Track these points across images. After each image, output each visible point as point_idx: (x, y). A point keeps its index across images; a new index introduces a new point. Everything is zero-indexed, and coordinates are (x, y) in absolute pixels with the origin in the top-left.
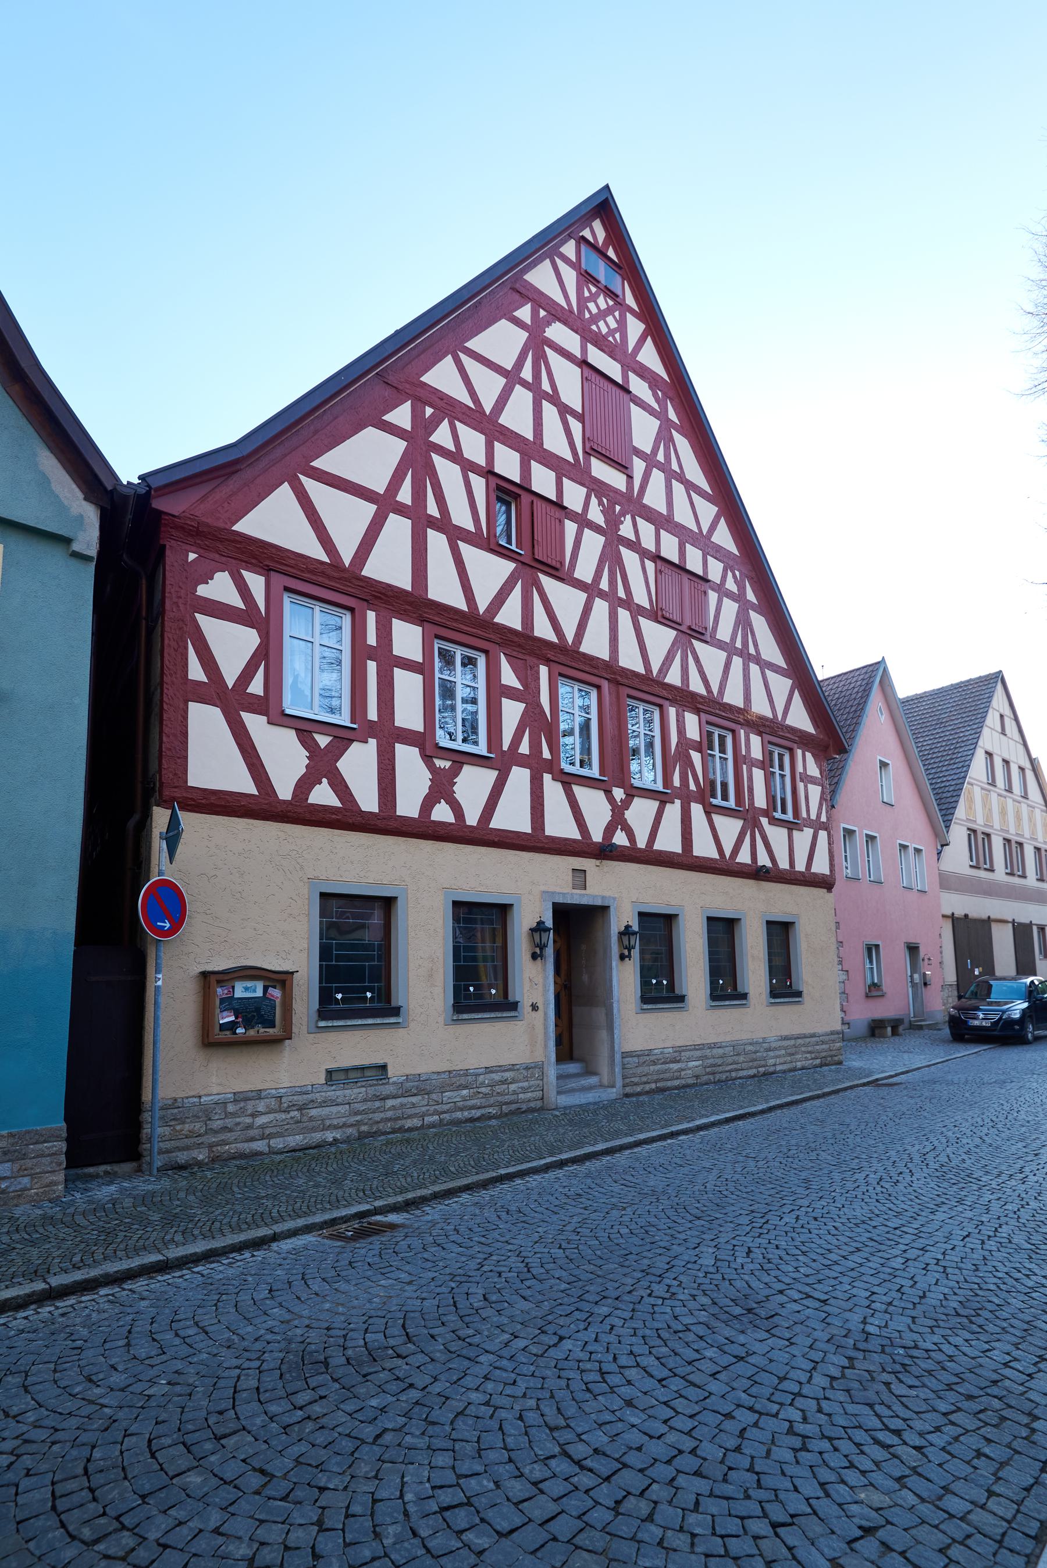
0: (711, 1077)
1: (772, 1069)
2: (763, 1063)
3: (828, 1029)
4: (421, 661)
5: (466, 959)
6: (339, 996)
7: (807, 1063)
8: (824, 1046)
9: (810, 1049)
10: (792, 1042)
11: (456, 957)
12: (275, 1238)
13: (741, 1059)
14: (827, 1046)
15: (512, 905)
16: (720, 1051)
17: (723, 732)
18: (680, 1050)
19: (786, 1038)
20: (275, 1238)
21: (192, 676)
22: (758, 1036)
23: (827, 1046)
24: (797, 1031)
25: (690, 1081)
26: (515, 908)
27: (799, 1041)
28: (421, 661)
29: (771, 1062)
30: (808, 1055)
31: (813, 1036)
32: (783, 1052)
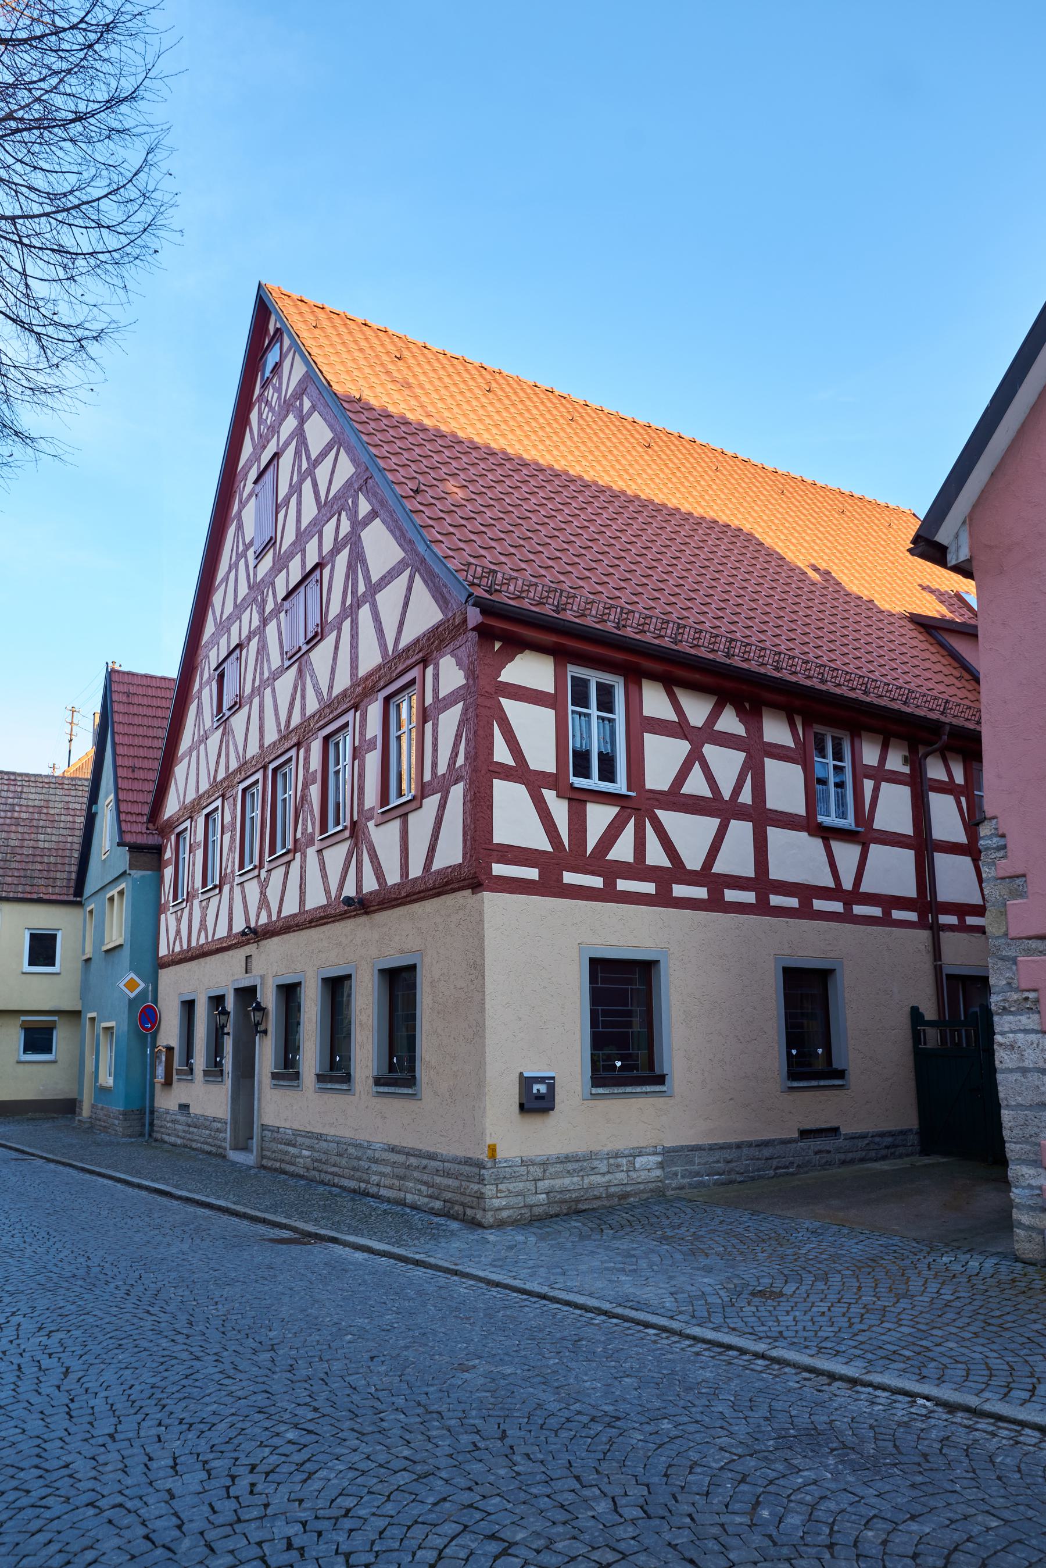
0: (316, 1173)
1: (373, 1190)
2: (365, 1177)
3: (460, 1153)
4: (553, 692)
5: (605, 1025)
6: (619, 1064)
7: (422, 1201)
8: (450, 1182)
9: (425, 1178)
10: (401, 1158)
11: (594, 1023)
12: (334, 1240)
13: (344, 1162)
14: (456, 1183)
15: (658, 962)
16: (324, 1144)
17: (607, 678)
18: (297, 1133)
19: (393, 1149)
20: (334, 1240)
21: (497, 758)
22: (363, 1136)
23: (456, 1183)
24: (409, 1142)
25: (301, 1171)
26: (838, 972)
27: (413, 1161)
28: (553, 692)
29: (375, 1179)
30: (424, 1188)
31: (432, 1157)
32: (388, 1170)
